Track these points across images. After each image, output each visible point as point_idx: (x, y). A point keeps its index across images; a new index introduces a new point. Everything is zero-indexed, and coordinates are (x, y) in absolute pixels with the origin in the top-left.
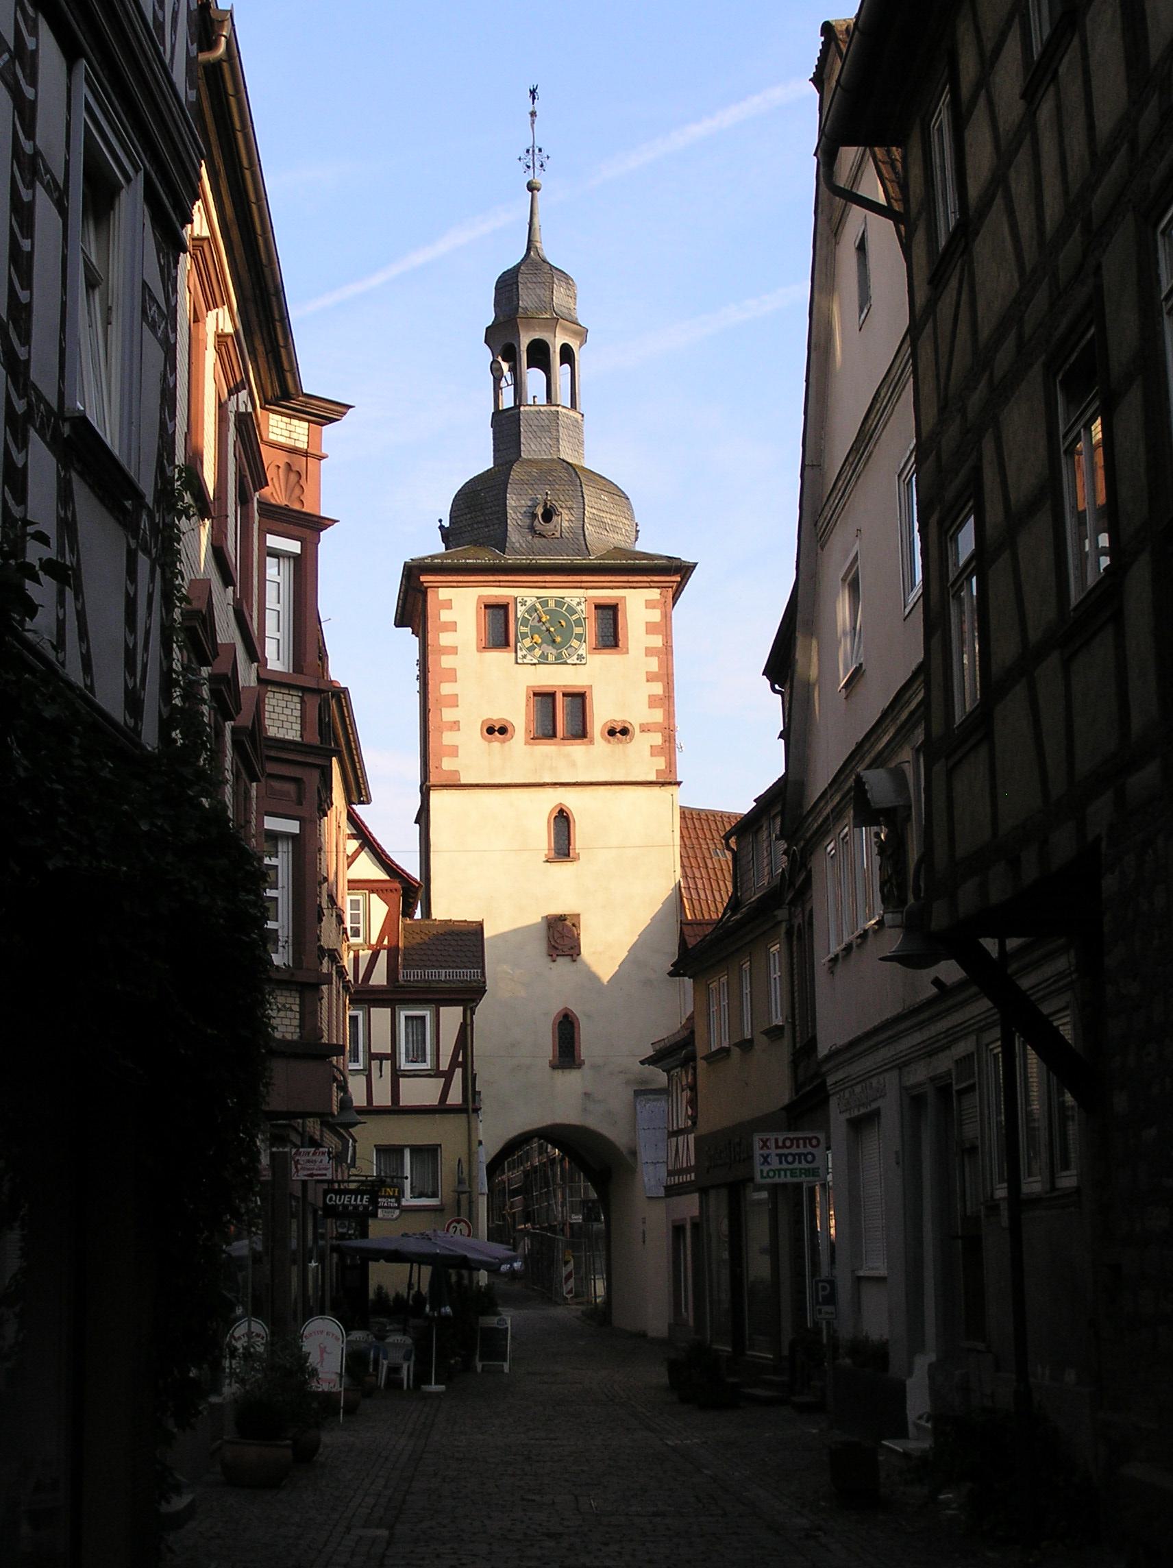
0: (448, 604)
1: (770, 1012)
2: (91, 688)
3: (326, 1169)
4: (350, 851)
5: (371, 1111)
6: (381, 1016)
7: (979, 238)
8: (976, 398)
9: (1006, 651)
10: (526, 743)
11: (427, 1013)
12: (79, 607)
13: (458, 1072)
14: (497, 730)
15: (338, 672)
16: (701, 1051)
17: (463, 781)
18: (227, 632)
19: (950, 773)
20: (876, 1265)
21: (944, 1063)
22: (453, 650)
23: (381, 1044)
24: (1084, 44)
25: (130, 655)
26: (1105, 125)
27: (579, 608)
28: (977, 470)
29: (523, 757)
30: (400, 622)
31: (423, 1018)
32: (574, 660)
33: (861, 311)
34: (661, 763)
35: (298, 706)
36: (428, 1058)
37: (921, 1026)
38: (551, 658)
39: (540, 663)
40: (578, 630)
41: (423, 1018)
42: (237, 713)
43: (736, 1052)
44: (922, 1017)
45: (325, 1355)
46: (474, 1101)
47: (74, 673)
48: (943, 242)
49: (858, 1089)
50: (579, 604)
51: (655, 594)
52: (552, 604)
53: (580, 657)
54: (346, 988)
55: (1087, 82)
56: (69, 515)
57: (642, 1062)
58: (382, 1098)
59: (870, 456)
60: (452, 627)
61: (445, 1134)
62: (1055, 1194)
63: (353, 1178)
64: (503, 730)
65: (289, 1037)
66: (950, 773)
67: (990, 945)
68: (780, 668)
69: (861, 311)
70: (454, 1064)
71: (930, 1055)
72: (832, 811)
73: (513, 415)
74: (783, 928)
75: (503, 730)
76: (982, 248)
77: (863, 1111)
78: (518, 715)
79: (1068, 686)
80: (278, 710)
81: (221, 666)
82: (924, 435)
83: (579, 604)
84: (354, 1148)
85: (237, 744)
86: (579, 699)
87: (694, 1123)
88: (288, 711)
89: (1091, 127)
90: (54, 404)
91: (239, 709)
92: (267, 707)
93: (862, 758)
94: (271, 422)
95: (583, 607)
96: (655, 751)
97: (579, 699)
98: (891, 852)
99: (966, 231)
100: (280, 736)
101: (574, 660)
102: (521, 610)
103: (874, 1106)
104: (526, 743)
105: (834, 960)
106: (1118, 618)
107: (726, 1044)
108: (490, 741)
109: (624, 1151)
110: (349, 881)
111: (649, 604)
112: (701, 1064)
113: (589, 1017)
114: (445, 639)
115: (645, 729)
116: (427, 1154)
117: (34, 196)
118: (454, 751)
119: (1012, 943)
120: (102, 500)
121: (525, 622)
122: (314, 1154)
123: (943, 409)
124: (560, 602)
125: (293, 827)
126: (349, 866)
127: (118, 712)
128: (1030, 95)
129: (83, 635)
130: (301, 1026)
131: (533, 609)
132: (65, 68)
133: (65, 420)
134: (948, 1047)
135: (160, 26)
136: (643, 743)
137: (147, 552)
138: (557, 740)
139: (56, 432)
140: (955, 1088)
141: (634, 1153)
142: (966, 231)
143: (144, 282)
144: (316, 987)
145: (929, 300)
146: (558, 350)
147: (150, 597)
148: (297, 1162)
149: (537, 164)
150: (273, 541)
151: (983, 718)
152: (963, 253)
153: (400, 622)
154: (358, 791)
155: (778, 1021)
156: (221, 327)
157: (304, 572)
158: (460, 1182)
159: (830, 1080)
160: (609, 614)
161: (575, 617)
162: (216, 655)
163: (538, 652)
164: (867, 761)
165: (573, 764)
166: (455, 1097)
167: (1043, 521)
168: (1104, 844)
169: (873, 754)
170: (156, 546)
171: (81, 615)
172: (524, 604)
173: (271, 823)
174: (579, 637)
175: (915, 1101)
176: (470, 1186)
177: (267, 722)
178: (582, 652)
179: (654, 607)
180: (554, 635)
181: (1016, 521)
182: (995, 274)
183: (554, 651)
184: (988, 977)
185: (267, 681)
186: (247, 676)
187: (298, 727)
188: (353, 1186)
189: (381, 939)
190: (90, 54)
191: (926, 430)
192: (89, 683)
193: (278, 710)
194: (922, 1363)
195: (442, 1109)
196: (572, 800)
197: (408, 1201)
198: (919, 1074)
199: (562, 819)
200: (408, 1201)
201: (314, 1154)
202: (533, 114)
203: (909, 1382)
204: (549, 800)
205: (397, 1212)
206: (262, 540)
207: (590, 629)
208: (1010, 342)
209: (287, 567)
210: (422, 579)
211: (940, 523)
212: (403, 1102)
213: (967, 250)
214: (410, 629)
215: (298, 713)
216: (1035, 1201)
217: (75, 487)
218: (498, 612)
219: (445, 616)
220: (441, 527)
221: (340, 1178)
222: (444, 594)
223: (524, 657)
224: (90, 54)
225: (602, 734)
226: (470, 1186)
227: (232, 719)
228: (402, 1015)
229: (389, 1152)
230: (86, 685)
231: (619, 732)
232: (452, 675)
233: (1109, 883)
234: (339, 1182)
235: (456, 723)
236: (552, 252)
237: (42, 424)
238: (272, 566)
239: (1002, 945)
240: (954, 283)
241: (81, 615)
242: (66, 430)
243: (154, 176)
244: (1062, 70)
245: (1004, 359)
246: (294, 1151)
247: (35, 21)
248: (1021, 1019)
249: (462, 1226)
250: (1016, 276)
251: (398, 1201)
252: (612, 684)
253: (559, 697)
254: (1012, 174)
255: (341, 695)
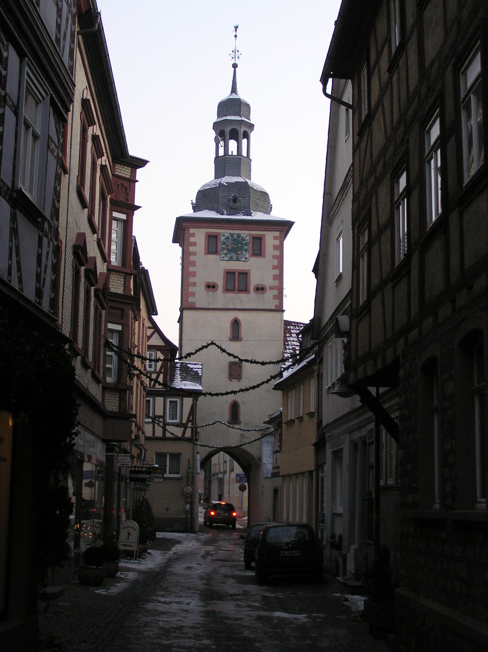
0: (193, 235)
1: (310, 407)
2: (22, 290)
3: (128, 462)
4: (149, 334)
5: (153, 439)
6: (159, 400)
7: (374, 121)
8: (371, 181)
9: (376, 281)
10: (223, 292)
11: (178, 400)
12: (18, 259)
13: (190, 425)
14: (211, 287)
15: (145, 262)
16: (284, 421)
17: (197, 306)
18: (93, 251)
19: (358, 323)
20: (340, 510)
21: (364, 432)
22: (195, 254)
23: (159, 412)
24: (407, 56)
25: (38, 276)
26: (412, 88)
27: (246, 238)
28: (370, 209)
29: (221, 298)
30: (175, 241)
31: (177, 402)
32: (243, 259)
33: (346, 135)
34: (277, 302)
35: (123, 280)
36: (178, 418)
37: (357, 417)
38: (234, 258)
39: (230, 260)
40: (246, 247)
41: (177, 402)
42: (96, 284)
43: (297, 421)
44: (358, 413)
45: (130, 536)
46: (196, 436)
47: (15, 284)
48: (363, 118)
49: (336, 440)
50: (246, 237)
51: (277, 234)
52: (235, 236)
53: (246, 258)
54: (144, 389)
55: (407, 71)
56: (15, 226)
57: (264, 423)
58: (159, 433)
59: (347, 193)
60: (194, 244)
61: (184, 449)
62: (397, 485)
63: (144, 466)
64: (213, 287)
65: (114, 410)
66: (358, 323)
67: (373, 390)
68: (316, 270)
69: (346, 135)
70: (188, 421)
71: (360, 428)
72: (330, 330)
73: (223, 159)
74: (316, 373)
75: (213, 287)
76: (375, 125)
77: (337, 448)
78: (220, 283)
79: (394, 295)
80: (115, 281)
81: (90, 266)
82: (355, 192)
83: (246, 237)
84: (145, 454)
85: (96, 295)
86: (245, 275)
87: (281, 449)
88: (119, 282)
89: (408, 87)
90: (10, 185)
91: (97, 282)
92: (111, 280)
93: (340, 310)
94: (117, 167)
95: (248, 238)
96: (275, 297)
97: (245, 275)
98: (347, 347)
99: (370, 117)
100: (115, 291)
101: (243, 259)
102: (223, 238)
103: (341, 447)
104: (223, 292)
105: (329, 388)
106: (409, 273)
107: (293, 418)
108: (208, 291)
109: (256, 458)
110: (148, 346)
111: (275, 238)
112: (284, 426)
113: (244, 403)
114: (192, 249)
115: (271, 288)
116: (176, 457)
117: (5, 111)
118: (193, 294)
119: (382, 390)
120: (29, 220)
121: (224, 243)
122: (124, 456)
123: (361, 183)
124: (239, 236)
125: (119, 328)
126: (148, 340)
127: (32, 297)
128: (390, 70)
129: (19, 269)
130: (120, 406)
131: (227, 238)
132: (19, 60)
133: (14, 191)
134: (365, 426)
135: (58, 40)
136: (270, 294)
137: (47, 236)
138: (236, 291)
139: (11, 195)
140: (368, 442)
141: (260, 459)
142: (370, 117)
143: (49, 136)
144: (125, 391)
145: (358, 141)
146: (242, 133)
147: (48, 253)
148: (117, 459)
149: (237, 57)
150: (115, 214)
151: (368, 304)
152: (369, 126)
153: (175, 241)
154: (152, 310)
155: (312, 410)
156: (95, 132)
157: (127, 226)
158: (189, 468)
159: (327, 435)
160: (259, 241)
161: (244, 242)
162: (87, 262)
163: (229, 256)
164: (342, 312)
165: (242, 302)
166: (188, 434)
167: (388, 233)
168: (401, 357)
169: (344, 309)
170: (51, 234)
171: (18, 263)
172: (224, 236)
173: (110, 326)
174: (246, 250)
175: (355, 445)
176: (193, 470)
177: (110, 286)
178: (247, 256)
179: (277, 239)
180: (236, 248)
181: (381, 231)
182: (378, 137)
183: (236, 256)
184: (370, 403)
185: (111, 270)
186: (101, 268)
187: (122, 288)
188: (144, 469)
189: (161, 369)
190: (29, 55)
191: (356, 190)
192: (21, 287)
193: (115, 281)
194: (354, 547)
195: (182, 439)
196: (241, 316)
197: (167, 475)
198: (356, 435)
199: (236, 323)
200: (167, 475)
201: (124, 456)
202: (236, 36)
203: (348, 555)
204: (231, 316)
205: (161, 480)
206: (111, 214)
207: (250, 247)
208: (381, 164)
209: (121, 225)
210: (184, 224)
211: (358, 227)
212: (168, 435)
213: (370, 125)
214: (178, 244)
215: (123, 283)
216: (387, 488)
217: (18, 216)
218: (212, 239)
219: (192, 240)
220: (192, 204)
221: (139, 465)
222: (192, 231)
223: (223, 257)
224: (29, 55)
225: (254, 290)
226: (193, 470)
227: (94, 286)
228: (168, 400)
229: (161, 456)
230: (20, 289)
231: (260, 289)
232: (194, 264)
233: (402, 372)
234: (139, 467)
235: (195, 283)
236: (242, 94)
237: (5, 193)
238: (114, 223)
239: (378, 390)
240: (366, 136)
241: (18, 263)
242: (15, 195)
243: (54, 96)
244: (400, 64)
245: (380, 168)
246: (116, 455)
247: (7, 46)
248: (383, 418)
249: (189, 487)
250: (384, 137)
251: (163, 475)
252: (257, 270)
253: (237, 274)
254: (384, 98)
255: (145, 273)
